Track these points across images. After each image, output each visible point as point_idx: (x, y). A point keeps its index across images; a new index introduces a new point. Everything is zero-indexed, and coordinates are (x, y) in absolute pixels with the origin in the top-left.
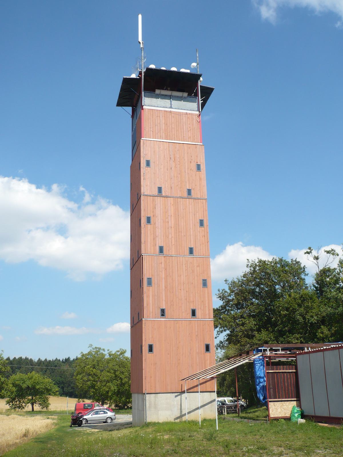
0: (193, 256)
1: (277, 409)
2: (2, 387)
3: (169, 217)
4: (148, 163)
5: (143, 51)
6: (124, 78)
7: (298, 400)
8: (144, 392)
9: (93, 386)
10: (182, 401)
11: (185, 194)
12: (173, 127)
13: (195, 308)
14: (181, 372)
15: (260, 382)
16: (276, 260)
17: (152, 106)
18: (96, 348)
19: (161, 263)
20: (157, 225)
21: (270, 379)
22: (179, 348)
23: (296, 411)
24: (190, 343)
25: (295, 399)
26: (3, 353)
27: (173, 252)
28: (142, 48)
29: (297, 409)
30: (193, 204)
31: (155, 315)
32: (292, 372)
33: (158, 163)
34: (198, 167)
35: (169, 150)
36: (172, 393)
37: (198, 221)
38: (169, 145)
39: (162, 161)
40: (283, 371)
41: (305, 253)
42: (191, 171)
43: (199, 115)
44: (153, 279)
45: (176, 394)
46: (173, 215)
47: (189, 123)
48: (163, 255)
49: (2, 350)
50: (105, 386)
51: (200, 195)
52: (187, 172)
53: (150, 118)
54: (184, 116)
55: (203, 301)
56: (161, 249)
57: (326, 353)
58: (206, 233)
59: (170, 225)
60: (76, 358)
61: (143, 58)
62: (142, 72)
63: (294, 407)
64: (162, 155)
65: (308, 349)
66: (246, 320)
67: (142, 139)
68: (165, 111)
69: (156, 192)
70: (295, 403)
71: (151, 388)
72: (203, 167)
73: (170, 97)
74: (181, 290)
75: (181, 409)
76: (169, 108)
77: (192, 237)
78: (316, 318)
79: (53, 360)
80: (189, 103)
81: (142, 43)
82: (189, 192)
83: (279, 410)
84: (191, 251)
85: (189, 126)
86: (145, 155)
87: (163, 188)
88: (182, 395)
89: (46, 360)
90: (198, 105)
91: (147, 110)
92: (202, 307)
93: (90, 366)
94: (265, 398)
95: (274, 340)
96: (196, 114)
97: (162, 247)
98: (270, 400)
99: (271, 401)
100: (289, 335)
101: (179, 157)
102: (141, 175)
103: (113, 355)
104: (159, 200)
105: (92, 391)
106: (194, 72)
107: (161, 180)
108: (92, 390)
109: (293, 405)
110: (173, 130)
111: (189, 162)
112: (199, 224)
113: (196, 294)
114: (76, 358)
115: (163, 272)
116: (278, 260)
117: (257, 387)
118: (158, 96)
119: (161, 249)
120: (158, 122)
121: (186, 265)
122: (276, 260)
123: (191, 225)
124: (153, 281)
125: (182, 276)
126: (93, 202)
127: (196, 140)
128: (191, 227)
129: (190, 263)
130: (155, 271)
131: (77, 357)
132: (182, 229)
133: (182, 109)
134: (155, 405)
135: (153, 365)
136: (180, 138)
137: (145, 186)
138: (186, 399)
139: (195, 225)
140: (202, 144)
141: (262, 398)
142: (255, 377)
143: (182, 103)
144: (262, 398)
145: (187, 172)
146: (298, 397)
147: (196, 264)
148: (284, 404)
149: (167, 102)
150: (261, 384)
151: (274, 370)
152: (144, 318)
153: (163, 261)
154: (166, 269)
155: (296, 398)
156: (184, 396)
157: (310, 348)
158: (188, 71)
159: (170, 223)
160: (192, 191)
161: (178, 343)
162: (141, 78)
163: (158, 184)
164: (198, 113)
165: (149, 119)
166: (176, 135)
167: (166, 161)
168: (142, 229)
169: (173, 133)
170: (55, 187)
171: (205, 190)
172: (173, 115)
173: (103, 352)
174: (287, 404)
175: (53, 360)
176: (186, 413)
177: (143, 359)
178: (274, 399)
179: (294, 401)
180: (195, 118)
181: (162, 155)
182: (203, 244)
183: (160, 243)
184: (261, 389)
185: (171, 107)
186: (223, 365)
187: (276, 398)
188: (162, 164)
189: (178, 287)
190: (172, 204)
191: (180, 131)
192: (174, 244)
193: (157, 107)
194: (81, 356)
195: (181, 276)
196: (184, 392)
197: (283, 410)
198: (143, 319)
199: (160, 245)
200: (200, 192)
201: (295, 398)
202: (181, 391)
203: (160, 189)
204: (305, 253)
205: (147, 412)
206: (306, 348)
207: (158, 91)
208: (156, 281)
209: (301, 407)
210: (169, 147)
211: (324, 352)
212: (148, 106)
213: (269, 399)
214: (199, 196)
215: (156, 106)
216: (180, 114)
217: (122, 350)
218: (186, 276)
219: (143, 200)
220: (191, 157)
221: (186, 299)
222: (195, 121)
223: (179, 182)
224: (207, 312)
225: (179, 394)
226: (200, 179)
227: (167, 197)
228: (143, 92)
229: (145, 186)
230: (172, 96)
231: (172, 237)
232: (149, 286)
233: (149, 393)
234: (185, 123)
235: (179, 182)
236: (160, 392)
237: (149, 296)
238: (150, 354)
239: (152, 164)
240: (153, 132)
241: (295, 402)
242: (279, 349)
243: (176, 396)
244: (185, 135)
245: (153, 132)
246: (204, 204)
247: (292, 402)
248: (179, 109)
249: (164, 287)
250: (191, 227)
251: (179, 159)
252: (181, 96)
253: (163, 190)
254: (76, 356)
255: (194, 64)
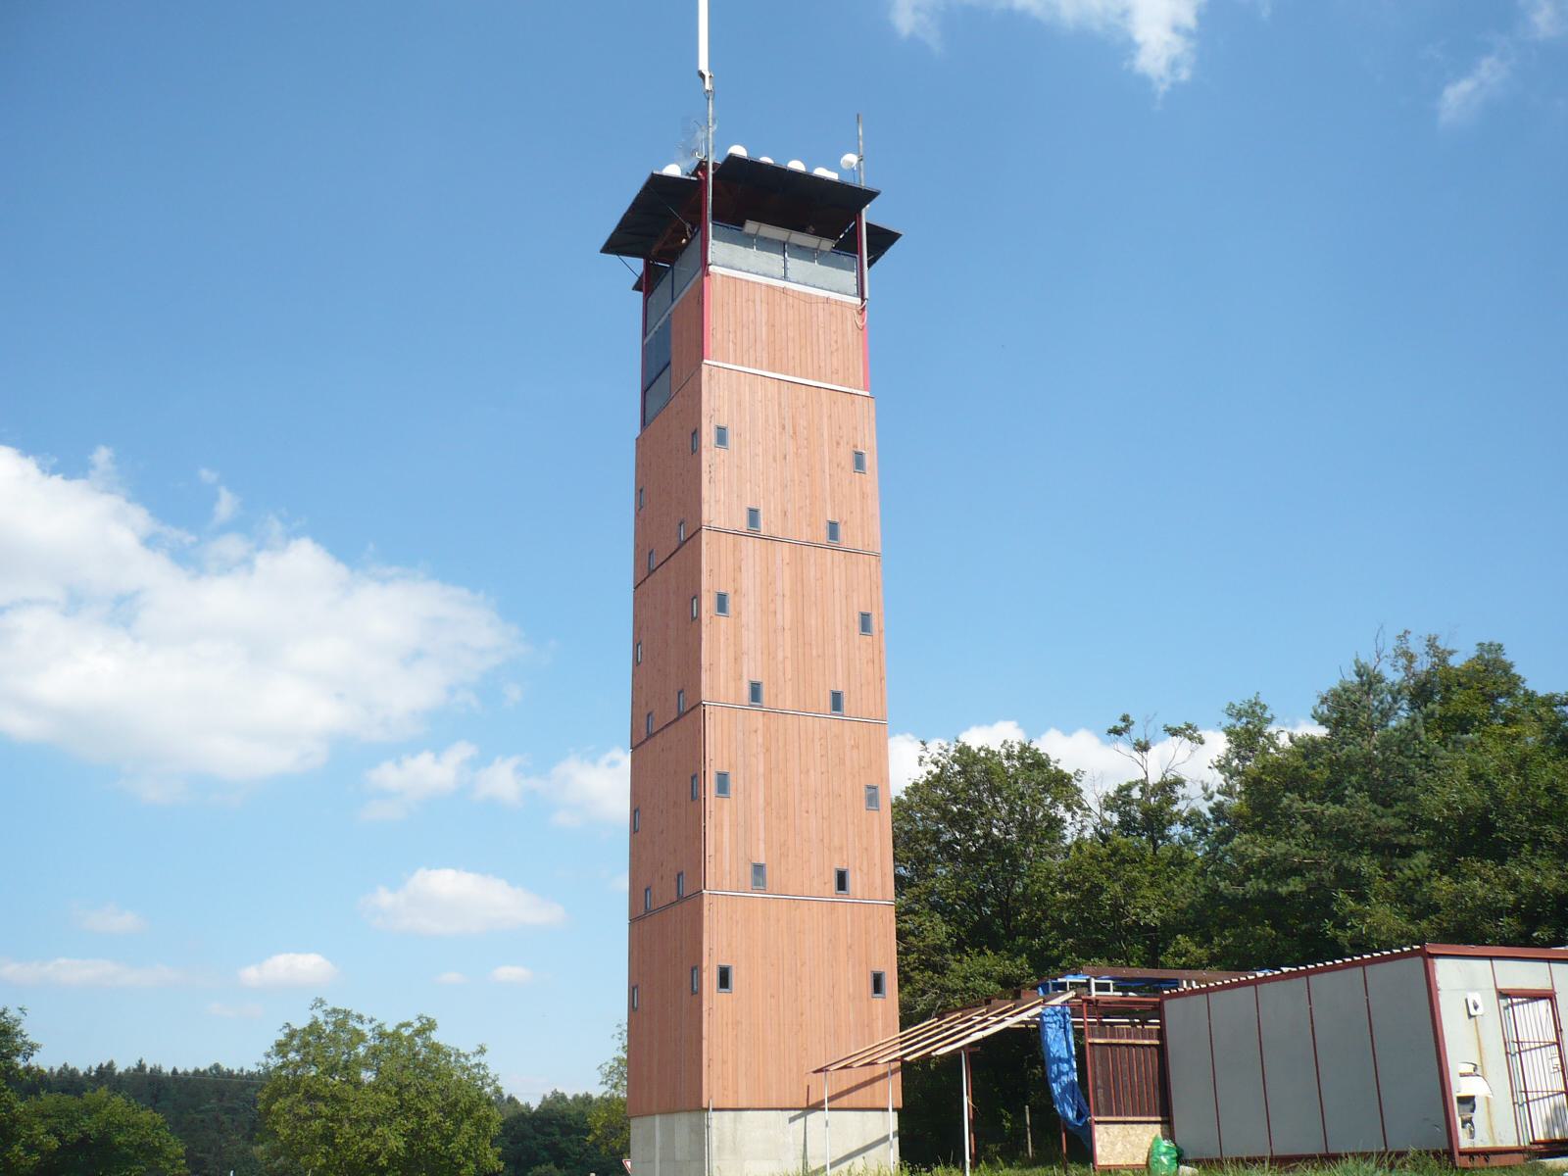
0: (842, 715)
1: (1113, 1144)
2: (13, 1134)
3: (778, 597)
4: (722, 436)
5: (710, 101)
6: (652, 174)
7: (1167, 1122)
8: (705, 1106)
9: (328, 1137)
10: (807, 1135)
11: (823, 535)
12: (791, 334)
13: (845, 868)
14: (806, 1049)
15: (1060, 1073)
16: (1011, 746)
17: (732, 268)
18: (335, 1011)
19: (756, 731)
20: (744, 619)
21: (1098, 1063)
22: (801, 981)
23: (1164, 1150)
24: (832, 966)
25: (1159, 1119)
26: (23, 1017)
27: (787, 702)
28: (708, 91)
29: (1165, 1145)
30: (843, 566)
31: (738, 880)
32: (1149, 1046)
33: (748, 438)
34: (859, 460)
35: (780, 404)
36: (782, 1109)
37: (857, 618)
38: (779, 387)
40: (1130, 1041)
41: (1110, 732)
42: (839, 470)
43: (863, 309)
44: (732, 778)
45: (793, 1113)
46: (788, 594)
47: (833, 328)
48: (761, 707)
49: (21, 1009)
50: (369, 1134)
51: (863, 541)
52: (827, 471)
53: (728, 304)
54: (821, 306)
56: (755, 691)
57: (1262, 987)
58: (877, 652)
60: (136, 1067)
61: (711, 121)
62: (707, 162)
63: (1156, 1139)
64: (760, 415)
65: (1189, 984)
66: (922, 919)
67: (705, 361)
68: (768, 286)
69: (741, 523)
70: (1158, 1127)
71: (726, 1093)
72: (870, 460)
73: (782, 247)
74: (807, 812)
75: (805, 1156)
76: (781, 279)
77: (839, 660)
78: (1156, 913)
79: (51, 1069)
80: (834, 269)
81: (710, 77)
82: (833, 529)
83: (1119, 1148)
84: (837, 700)
85: (835, 338)
86: (714, 410)
87: (761, 512)
88: (808, 1117)
90: (859, 278)
91: (719, 278)
92: (865, 863)
93: (321, 1069)
94: (1080, 1116)
95: (1031, 975)
96: (851, 304)
97: (758, 684)
98: (1097, 1119)
99: (1098, 1123)
100: (1077, 960)
101: (805, 424)
103: (389, 1036)
104: (749, 545)
105: (322, 1153)
106: (849, 180)
108: (324, 1148)
109: (1154, 1136)
110: (790, 344)
111: (835, 444)
112: (857, 626)
113: (849, 826)
114: (136, 1067)
115: (761, 757)
116: (1017, 749)
117: (1054, 1085)
118: (748, 241)
119: (755, 691)
120: (751, 318)
122: (1011, 746)
123: (838, 627)
124: (734, 783)
125: (812, 772)
126: (240, 525)
127: (851, 380)
128: (838, 635)
130: (740, 753)
131: (140, 1061)
132: (813, 638)
133: (814, 286)
134: (735, 1144)
135: (730, 1026)
136: (810, 370)
137: (713, 503)
138: (827, 1125)
139: (847, 628)
140: (867, 394)
141: (1071, 1115)
142: (1046, 1058)
143: (815, 267)
144: (1071, 1115)
145: (827, 471)
146: (1166, 1116)
147: (850, 740)
148: (1131, 1132)
149: (772, 261)
150: (1065, 1079)
151: (1106, 1037)
152: (707, 887)
154: (767, 750)
155: (1161, 1116)
156: (814, 1118)
157: (1194, 983)
158: (833, 176)
159: (779, 616)
160: (842, 530)
161: (799, 965)
162: (702, 184)
163: (749, 500)
164: (858, 301)
165: (725, 305)
166: (797, 357)
167: (771, 435)
168: (704, 628)
169: (791, 353)
170: (102, 455)
171: (875, 528)
172: (790, 300)
173: (359, 1027)
174: (1138, 1132)
175: (51, 1069)
176: (831, 1167)
177: (704, 1009)
178: (1107, 1115)
179: (1155, 1122)
180: (849, 317)
181: (760, 415)
182: (869, 684)
183: (752, 671)
184: (1064, 1090)
185: (785, 278)
186: (920, 1038)
187: (1111, 1115)
188: (760, 440)
189: (801, 802)
190: (785, 562)
191: (809, 350)
192: (790, 680)
193: (748, 272)
194: (286, 1035)
195: (808, 771)
196: (818, 1107)
197: (1128, 1146)
199: (753, 680)
200: (863, 532)
201: (1156, 1115)
202: (805, 1106)
203: (753, 514)
204: (1110, 732)
205: (714, 1164)
206: (1185, 983)
207: (751, 227)
208: (741, 782)
209: (1174, 1142)
210: (779, 393)
211: (1210, 994)
212: (723, 266)
213: (1095, 1115)
214: (860, 543)
215: (743, 269)
216: (809, 300)
217: (424, 1021)
218: (822, 773)
219: (707, 544)
220: (840, 428)
221: (822, 840)
222: (849, 324)
223: (806, 498)
224: (878, 881)
225: (799, 1112)
226: (863, 495)
227: (773, 539)
228: (711, 225)
229: (713, 503)
230: (789, 244)
231: (785, 658)
232: (720, 795)
233: (721, 1106)
235: (806, 498)
236: (749, 1106)
237: (722, 825)
238: (723, 996)
239: (732, 439)
240: (735, 344)
242: (1109, 984)
243: (792, 1120)
244: (822, 364)
245: (735, 344)
246: (873, 566)
247: (1151, 1126)
248: (805, 284)
249: (761, 801)
250: (838, 635)
251: (805, 432)
252: (815, 246)
253: (762, 517)
255: (851, 159)
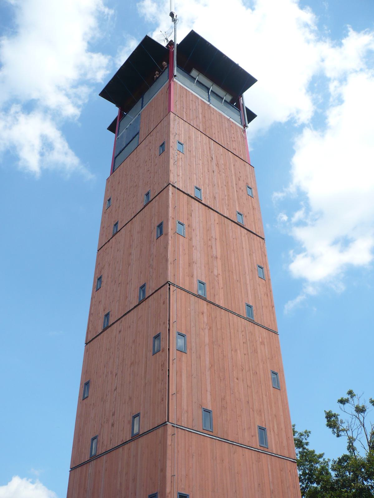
39: (200, 155)
55: (276, 416)
59: (214, 253)
89: (339, 458)
102: (171, 157)
107: (200, 180)
121: (243, 333)
129: (250, 332)
153: (205, 311)
188: (201, 158)
198: (167, 423)
208: (213, 148)
234: (230, 118)
241: (138, 430)
254: (321, 453)
